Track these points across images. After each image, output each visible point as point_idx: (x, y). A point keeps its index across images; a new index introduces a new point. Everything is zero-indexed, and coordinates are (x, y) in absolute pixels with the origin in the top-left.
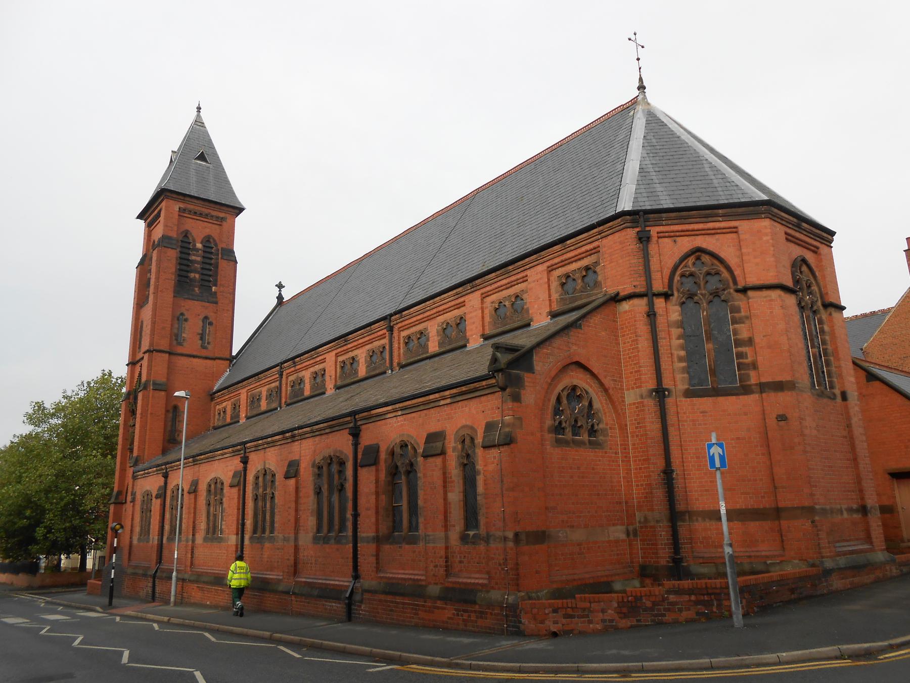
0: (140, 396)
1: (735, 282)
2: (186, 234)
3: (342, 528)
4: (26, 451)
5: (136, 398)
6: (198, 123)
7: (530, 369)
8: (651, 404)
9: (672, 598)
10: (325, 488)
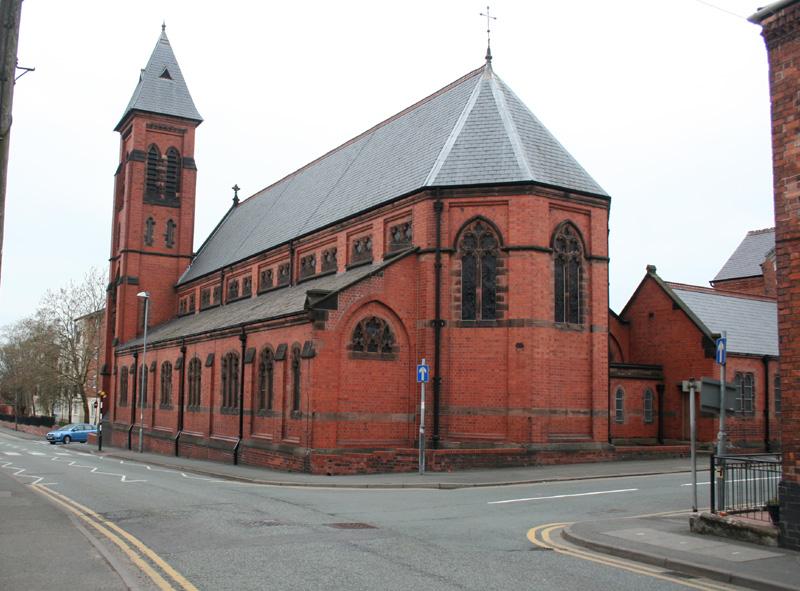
0: (119, 288)
1: (502, 244)
2: (154, 147)
3: (236, 406)
4: (10, 352)
5: (116, 290)
6: (164, 41)
7: (334, 307)
8: (430, 330)
9: (399, 458)
10: (228, 375)
